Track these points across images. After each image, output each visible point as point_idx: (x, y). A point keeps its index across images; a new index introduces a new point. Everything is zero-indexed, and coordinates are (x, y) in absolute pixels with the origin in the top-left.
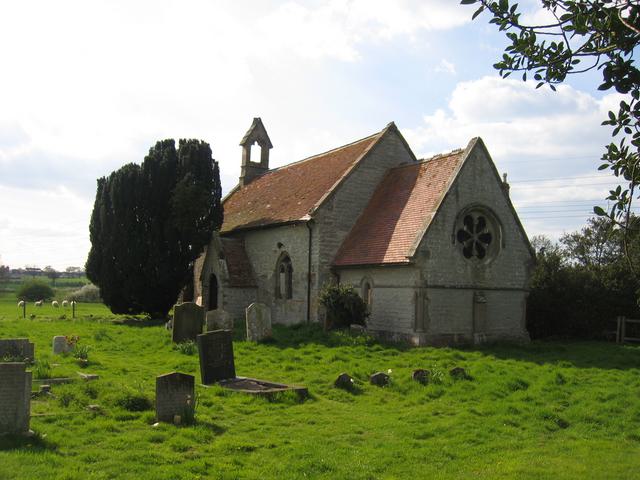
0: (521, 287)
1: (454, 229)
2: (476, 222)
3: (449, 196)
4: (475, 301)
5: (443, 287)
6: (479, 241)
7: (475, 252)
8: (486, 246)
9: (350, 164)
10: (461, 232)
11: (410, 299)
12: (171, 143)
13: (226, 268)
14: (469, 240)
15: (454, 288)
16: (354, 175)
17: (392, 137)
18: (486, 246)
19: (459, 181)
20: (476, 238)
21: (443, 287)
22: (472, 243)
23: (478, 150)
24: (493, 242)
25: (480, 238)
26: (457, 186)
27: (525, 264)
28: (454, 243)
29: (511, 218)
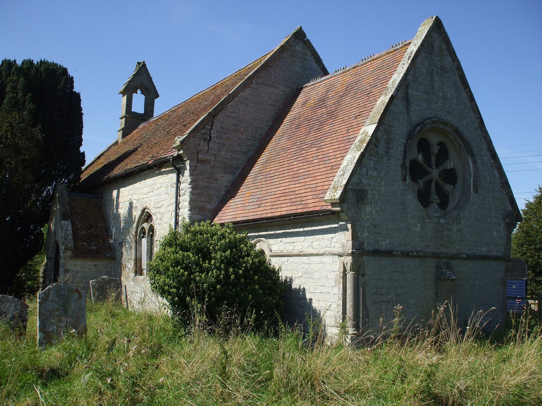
0: (500, 254)
1: (404, 158)
2: (435, 149)
3: (395, 101)
4: (439, 277)
5: (389, 253)
6: (441, 183)
7: (435, 198)
8: (448, 188)
9: (242, 79)
10: (414, 163)
11: (332, 276)
12: (10, 60)
13: (70, 232)
14: (427, 178)
15: (405, 254)
16: (248, 92)
17: (299, 47)
18: (448, 188)
19: (410, 77)
20: (435, 173)
21: (389, 253)
22: (428, 184)
23: (435, 35)
24: (459, 184)
25: (440, 176)
26: (407, 86)
27: (504, 218)
28: (404, 180)
29: (485, 147)
